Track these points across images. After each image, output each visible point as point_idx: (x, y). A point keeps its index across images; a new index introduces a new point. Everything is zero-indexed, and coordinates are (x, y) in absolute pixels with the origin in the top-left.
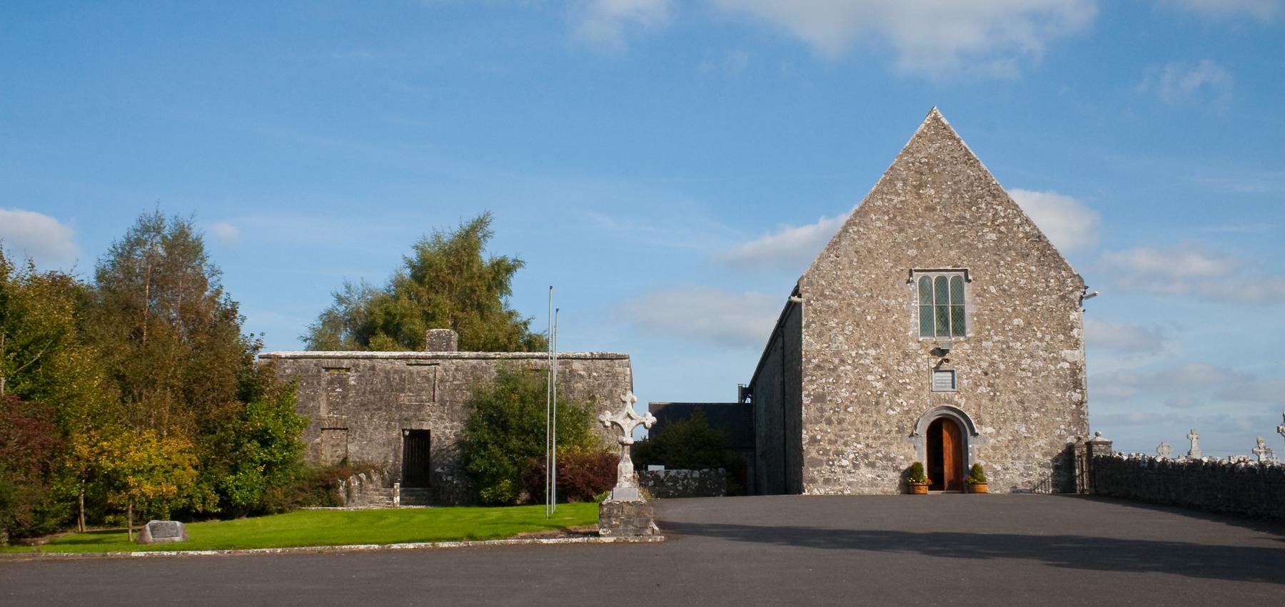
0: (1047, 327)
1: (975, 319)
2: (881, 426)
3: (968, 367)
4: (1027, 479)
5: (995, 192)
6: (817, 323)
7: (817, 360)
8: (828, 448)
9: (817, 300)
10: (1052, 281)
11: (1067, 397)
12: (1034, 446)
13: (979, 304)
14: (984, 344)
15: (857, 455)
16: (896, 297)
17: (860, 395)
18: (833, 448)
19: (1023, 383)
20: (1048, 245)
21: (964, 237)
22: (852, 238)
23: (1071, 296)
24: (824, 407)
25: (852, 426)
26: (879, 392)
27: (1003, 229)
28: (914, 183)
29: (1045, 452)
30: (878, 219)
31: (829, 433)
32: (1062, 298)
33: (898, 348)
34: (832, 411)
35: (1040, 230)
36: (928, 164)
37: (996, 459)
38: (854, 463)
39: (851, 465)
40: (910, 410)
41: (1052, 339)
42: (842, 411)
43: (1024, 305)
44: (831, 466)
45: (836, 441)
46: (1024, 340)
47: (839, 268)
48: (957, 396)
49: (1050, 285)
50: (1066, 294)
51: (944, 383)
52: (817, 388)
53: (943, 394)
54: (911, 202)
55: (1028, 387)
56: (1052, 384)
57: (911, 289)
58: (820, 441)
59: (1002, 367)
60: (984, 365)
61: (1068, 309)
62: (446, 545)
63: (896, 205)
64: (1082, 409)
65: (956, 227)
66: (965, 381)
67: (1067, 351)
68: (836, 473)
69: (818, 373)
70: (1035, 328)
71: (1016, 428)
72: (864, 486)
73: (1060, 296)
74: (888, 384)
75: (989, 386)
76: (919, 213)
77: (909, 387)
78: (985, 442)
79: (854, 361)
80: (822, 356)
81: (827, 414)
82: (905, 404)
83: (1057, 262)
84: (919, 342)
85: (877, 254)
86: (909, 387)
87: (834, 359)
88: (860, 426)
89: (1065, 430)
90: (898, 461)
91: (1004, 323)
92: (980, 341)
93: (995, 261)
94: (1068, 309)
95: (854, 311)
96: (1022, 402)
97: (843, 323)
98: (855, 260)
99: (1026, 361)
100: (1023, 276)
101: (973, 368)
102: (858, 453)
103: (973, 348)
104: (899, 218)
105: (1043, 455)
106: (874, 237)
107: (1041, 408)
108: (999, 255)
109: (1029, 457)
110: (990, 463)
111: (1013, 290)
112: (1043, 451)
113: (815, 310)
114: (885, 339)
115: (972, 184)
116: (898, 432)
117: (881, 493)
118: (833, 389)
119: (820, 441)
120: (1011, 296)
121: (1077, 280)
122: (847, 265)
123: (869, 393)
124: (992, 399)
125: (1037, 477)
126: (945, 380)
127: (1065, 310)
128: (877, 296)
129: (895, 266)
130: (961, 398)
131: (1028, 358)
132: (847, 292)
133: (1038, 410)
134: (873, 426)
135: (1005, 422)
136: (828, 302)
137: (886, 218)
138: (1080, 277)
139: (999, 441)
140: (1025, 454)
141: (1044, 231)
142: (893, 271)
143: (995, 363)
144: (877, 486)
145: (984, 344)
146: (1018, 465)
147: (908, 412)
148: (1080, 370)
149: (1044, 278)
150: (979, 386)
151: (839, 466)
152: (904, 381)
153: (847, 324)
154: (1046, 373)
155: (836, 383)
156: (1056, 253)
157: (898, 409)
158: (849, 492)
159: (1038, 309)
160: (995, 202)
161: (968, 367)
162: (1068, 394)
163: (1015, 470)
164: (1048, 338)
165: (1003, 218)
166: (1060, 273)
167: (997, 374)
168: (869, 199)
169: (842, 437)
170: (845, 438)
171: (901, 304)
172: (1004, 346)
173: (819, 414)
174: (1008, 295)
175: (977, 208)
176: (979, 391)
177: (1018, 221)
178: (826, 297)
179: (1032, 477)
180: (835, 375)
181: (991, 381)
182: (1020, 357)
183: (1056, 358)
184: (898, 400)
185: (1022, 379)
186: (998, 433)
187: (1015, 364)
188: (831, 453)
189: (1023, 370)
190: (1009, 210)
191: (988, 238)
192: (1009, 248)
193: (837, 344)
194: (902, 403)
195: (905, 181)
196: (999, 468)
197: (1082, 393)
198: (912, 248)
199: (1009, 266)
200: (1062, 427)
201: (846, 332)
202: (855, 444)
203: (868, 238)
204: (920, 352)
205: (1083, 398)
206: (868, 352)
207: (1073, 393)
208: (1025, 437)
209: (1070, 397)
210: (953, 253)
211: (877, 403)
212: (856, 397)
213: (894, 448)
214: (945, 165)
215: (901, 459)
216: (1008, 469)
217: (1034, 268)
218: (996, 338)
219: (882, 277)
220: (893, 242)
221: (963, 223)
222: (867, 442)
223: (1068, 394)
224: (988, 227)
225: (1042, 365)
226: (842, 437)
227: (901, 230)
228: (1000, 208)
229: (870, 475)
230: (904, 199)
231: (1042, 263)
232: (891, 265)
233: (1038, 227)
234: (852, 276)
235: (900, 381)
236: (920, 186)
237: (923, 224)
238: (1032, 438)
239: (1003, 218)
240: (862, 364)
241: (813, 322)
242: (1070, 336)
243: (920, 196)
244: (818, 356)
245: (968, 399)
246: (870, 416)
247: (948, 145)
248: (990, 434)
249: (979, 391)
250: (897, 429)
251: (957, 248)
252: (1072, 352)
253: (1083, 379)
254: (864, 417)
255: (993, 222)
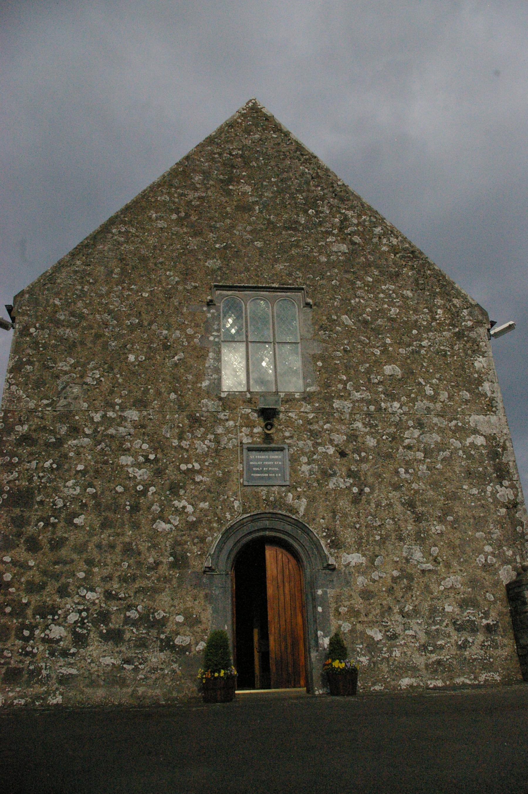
0: (439, 379)
1: (320, 364)
2: (139, 554)
3: (310, 443)
4: (434, 657)
5: (343, 194)
6: (37, 363)
7: (26, 427)
8: (25, 601)
9: (42, 328)
10: (440, 311)
11: (488, 493)
12: (442, 588)
13: (324, 341)
14: (337, 404)
15: (84, 614)
16: (182, 327)
17: (102, 493)
18: (35, 599)
19: (411, 471)
20: (426, 264)
21: (297, 246)
22: (115, 240)
23: (473, 335)
24: (26, 514)
25: (80, 552)
26: (140, 488)
27: (357, 239)
28: (221, 177)
29: (464, 600)
30: (161, 218)
31: (31, 568)
32: (459, 336)
33: (181, 408)
34: (42, 524)
35: (413, 243)
36: (241, 156)
37: (370, 617)
38: (75, 633)
39: (70, 637)
40: (199, 521)
41: (450, 398)
42: (62, 524)
43: (400, 344)
44: (26, 640)
45: (42, 587)
46: (404, 399)
47: (88, 281)
48: (290, 495)
49: (437, 317)
50: (463, 330)
51: (268, 472)
52: (17, 479)
53: (263, 492)
54: (215, 200)
55: (419, 478)
56: (461, 472)
57: (209, 315)
58: (9, 585)
59: (371, 442)
60: (339, 438)
61: (469, 352)
62: (256, 638)
63: (191, 201)
64: (517, 515)
65: (284, 232)
66: (305, 468)
67: (477, 417)
68: (34, 655)
69: (24, 451)
70: (421, 380)
71: (405, 554)
72: (93, 684)
73: (455, 334)
74: (159, 473)
75: (349, 476)
76: (227, 213)
77: (198, 478)
78: (348, 582)
79: (95, 431)
80: (36, 420)
81: (30, 530)
82: (190, 509)
83: (444, 285)
84: (220, 399)
85: (156, 264)
86: (198, 478)
87: (58, 425)
88: (96, 554)
89: (493, 554)
90: (170, 627)
91: (368, 372)
92: (329, 399)
93: (348, 280)
94: (469, 352)
95: (105, 346)
96: (411, 505)
97: (84, 365)
98: (117, 270)
99: (412, 433)
100: (394, 303)
101: (319, 444)
102: (87, 610)
103: (317, 411)
104: (193, 218)
105: (461, 607)
106: (152, 241)
107: (446, 515)
108: (354, 273)
109: (433, 611)
110: (359, 627)
111: (379, 322)
112: (457, 597)
113: (37, 343)
114: (159, 393)
115: (307, 183)
116: (173, 565)
117: (131, 701)
118: (50, 481)
119: (9, 585)
120: (377, 331)
121: (477, 312)
122: (103, 277)
123: (120, 489)
124: (356, 500)
125: (454, 651)
126: (269, 466)
127: (467, 354)
128: (150, 324)
129: (184, 281)
130: (299, 498)
131: (414, 427)
132: (98, 316)
133: (441, 520)
134: (123, 555)
135: (384, 540)
136: (60, 331)
137: (174, 217)
138: (481, 309)
139: (374, 581)
140: (426, 605)
141: (418, 245)
142: (180, 288)
143: (357, 437)
144: (123, 682)
145: (337, 404)
146: (416, 628)
147: (193, 526)
148: (504, 448)
149: (427, 308)
150: (331, 475)
151: (44, 640)
152: (190, 466)
153: (91, 366)
154: (447, 453)
155: (57, 469)
156: (439, 276)
157: (176, 521)
158: (59, 699)
159: (423, 352)
160: (342, 206)
161: (310, 443)
162: (489, 489)
163: (410, 639)
164: (444, 396)
165: (357, 225)
166: (450, 301)
167: (363, 454)
168: (149, 192)
169: (56, 577)
170: (63, 580)
171: (190, 338)
172: (372, 408)
173: (15, 530)
174: (373, 330)
175: (316, 211)
176: (331, 486)
177: (378, 230)
178: (58, 323)
179: (445, 652)
180: (57, 454)
181: (353, 468)
182: (400, 425)
183: (463, 428)
184: (176, 503)
185: (408, 464)
186: (372, 564)
187: (394, 438)
188: (29, 612)
189: (409, 447)
190: (364, 217)
191: (335, 249)
192: (368, 265)
193: (69, 400)
194: (184, 507)
195: (206, 174)
196: (379, 636)
197: (513, 487)
198: (214, 257)
199: (371, 288)
200: (488, 549)
201: (89, 380)
202: (83, 592)
203: (142, 242)
204: (222, 416)
205: (516, 496)
206: (125, 414)
207: (498, 487)
208: (423, 571)
209: (494, 494)
210: (279, 267)
211: (135, 508)
212: (94, 496)
213: (164, 598)
214: (268, 159)
215: (178, 623)
216: (395, 637)
217: (409, 294)
218: (357, 395)
219: (161, 296)
220: (182, 249)
221: (295, 229)
222: (108, 586)
223: (489, 489)
224: (333, 235)
225: (439, 439)
226: (56, 577)
227: (195, 235)
228: (350, 213)
229: (108, 660)
230: (204, 195)
231: (421, 287)
232: (177, 279)
233: (409, 239)
234: (109, 293)
235: (183, 467)
236: (230, 181)
237: (233, 227)
238: (435, 572)
239: (357, 225)
240: (112, 436)
241: (29, 362)
242: (479, 393)
243: (229, 193)
244: (28, 420)
245: (312, 500)
246: (118, 535)
247: (272, 137)
248: (358, 566)
249: (331, 486)
250: (171, 559)
251: (286, 261)
252: (486, 418)
253: (511, 463)
254: (105, 537)
255: (341, 229)
